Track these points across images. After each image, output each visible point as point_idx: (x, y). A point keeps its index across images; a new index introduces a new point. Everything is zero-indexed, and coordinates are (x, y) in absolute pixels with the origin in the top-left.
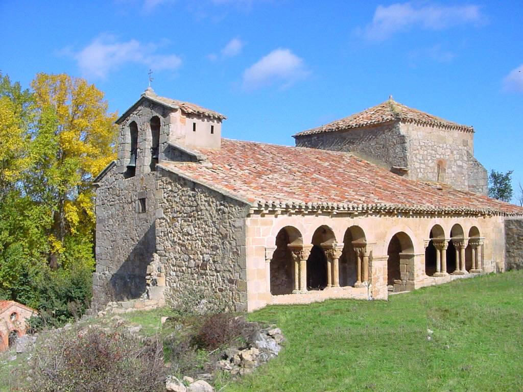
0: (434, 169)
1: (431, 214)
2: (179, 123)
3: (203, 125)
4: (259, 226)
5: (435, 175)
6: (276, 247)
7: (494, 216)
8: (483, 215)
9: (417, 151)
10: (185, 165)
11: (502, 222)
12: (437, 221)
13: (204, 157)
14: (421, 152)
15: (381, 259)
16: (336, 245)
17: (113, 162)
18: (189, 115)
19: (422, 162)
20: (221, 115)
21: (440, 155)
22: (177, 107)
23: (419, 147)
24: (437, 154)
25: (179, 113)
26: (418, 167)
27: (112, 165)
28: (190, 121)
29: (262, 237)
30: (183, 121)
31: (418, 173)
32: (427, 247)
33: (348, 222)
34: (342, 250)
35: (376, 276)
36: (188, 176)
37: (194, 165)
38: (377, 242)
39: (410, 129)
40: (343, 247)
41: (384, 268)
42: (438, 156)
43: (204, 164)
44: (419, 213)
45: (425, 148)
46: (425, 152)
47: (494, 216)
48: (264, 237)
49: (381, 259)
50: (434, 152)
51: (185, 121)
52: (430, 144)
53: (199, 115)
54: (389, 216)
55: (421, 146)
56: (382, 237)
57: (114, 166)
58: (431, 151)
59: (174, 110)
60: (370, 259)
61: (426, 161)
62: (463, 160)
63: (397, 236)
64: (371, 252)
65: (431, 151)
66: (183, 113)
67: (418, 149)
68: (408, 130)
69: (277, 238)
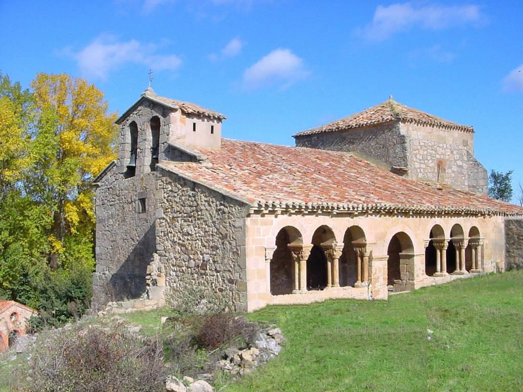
0: (434, 169)
1: (431, 214)
3: (203, 125)
4: (259, 226)
5: (435, 175)
6: (276, 247)
8: (483, 215)
9: (417, 151)
11: (502, 222)
13: (204, 157)
14: (421, 152)
15: (381, 259)
16: (336, 245)
17: (113, 162)
18: (189, 115)
20: (221, 115)
21: (440, 155)
22: (177, 107)
23: (419, 147)
24: (437, 154)
25: (179, 113)
26: (418, 167)
27: (112, 166)
28: (190, 121)
29: (262, 237)
30: (183, 121)
32: (427, 247)
34: (342, 250)
37: (194, 165)
38: (377, 242)
40: (343, 247)
41: (384, 268)
42: (438, 156)
43: (204, 164)
44: (419, 213)
45: (425, 148)
46: (425, 152)
48: (264, 237)
49: (381, 259)
53: (199, 115)
54: (389, 216)
55: (421, 146)
57: (114, 166)
58: (431, 151)
60: (370, 259)
61: (426, 161)
62: (463, 160)
63: (398, 236)
64: (371, 252)
65: (431, 151)
66: (183, 113)
67: (418, 149)
69: (277, 238)
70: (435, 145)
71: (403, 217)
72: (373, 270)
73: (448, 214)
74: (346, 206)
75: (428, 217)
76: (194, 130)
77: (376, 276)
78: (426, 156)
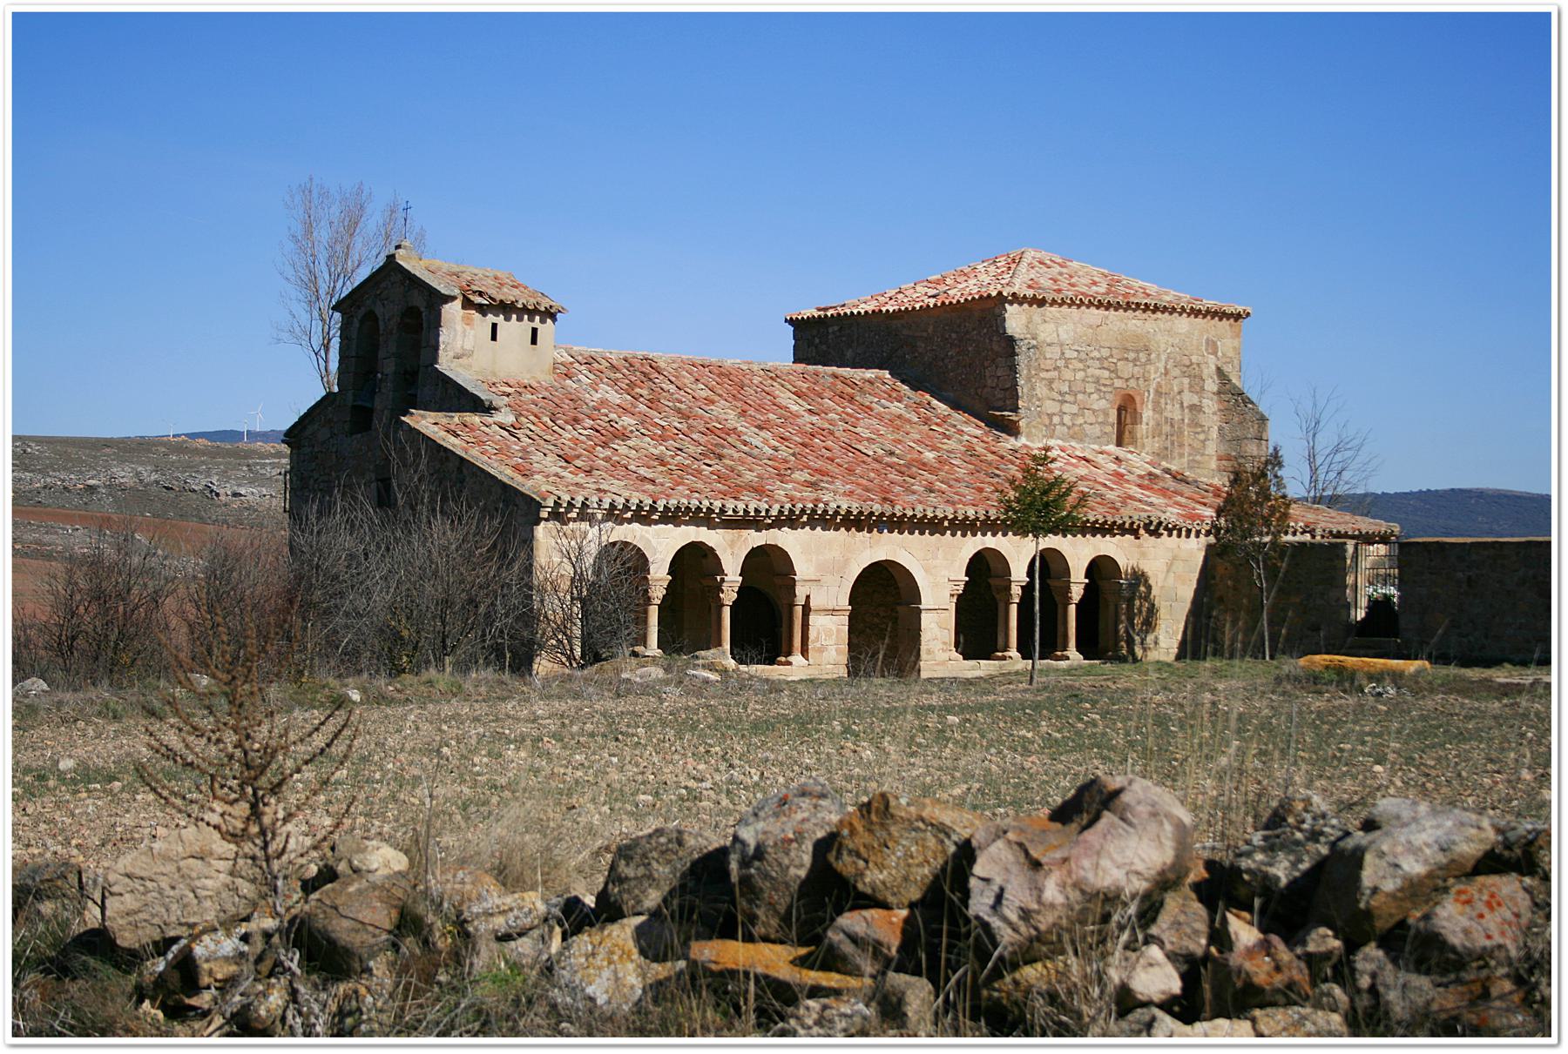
1: (965, 526)
2: (459, 327)
3: (514, 330)
7: (1170, 535)
8: (1134, 532)
9: (1056, 373)
10: (456, 420)
11: (1199, 549)
12: (633, 533)
13: (498, 402)
14: (1068, 375)
15: (833, 612)
16: (723, 580)
18: (483, 310)
19: (1068, 398)
20: (554, 299)
21: (1127, 380)
22: (456, 292)
23: (1061, 363)
24: (1119, 377)
25: (457, 305)
26: (1056, 410)
28: (484, 323)
30: (468, 321)
31: (1055, 425)
32: (959, 596)
33: (755, 538)
34: (736, 589)
35: (818, 645)
36: (453, 445)
37: (475, 419)
38: (824, 579)
39: (1037, 319)
41: (838, 631)
42: (1118, 383)
43: (499, 417)
44: (933, 526)
46: (1080, 375)
47: (1170, 535)
49: (833, 612)
50: (1106, 374)
51: (472, 320)
52: (1096, 354)
53: (506, 309)
54: (823, 529)
56: (840, 568)
58: (1098, 372)
59: (453, 298)
60: (807, 609)
61: (1080, 397)
64: (808, 597)
65: (1098, 372)
66: (467, 304)
67: (1056, 369)
68: (1030, 321)
70: (1112, 356)
71: (819, 528)
72: (812, 634)
73: (672, 517)
74: (741, 506)
75: (953, 535)
76: (494, 338)
77: (818, 645)
78: (1079, 383)
